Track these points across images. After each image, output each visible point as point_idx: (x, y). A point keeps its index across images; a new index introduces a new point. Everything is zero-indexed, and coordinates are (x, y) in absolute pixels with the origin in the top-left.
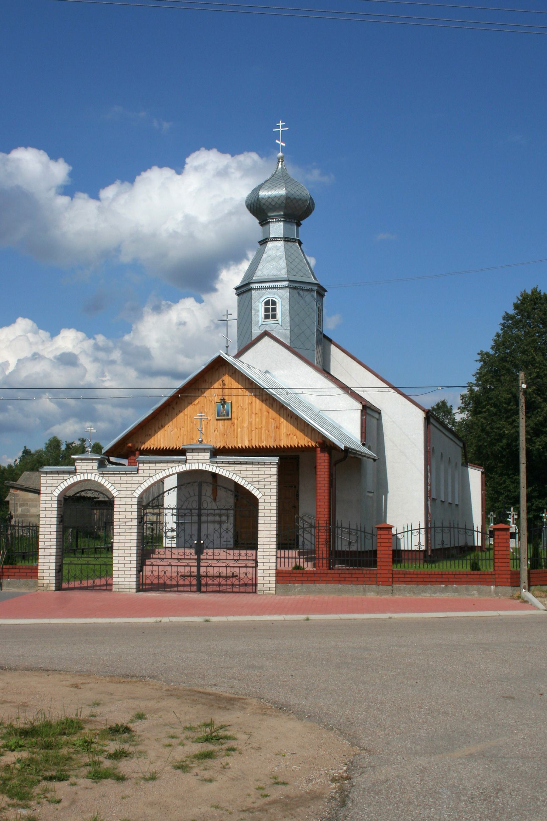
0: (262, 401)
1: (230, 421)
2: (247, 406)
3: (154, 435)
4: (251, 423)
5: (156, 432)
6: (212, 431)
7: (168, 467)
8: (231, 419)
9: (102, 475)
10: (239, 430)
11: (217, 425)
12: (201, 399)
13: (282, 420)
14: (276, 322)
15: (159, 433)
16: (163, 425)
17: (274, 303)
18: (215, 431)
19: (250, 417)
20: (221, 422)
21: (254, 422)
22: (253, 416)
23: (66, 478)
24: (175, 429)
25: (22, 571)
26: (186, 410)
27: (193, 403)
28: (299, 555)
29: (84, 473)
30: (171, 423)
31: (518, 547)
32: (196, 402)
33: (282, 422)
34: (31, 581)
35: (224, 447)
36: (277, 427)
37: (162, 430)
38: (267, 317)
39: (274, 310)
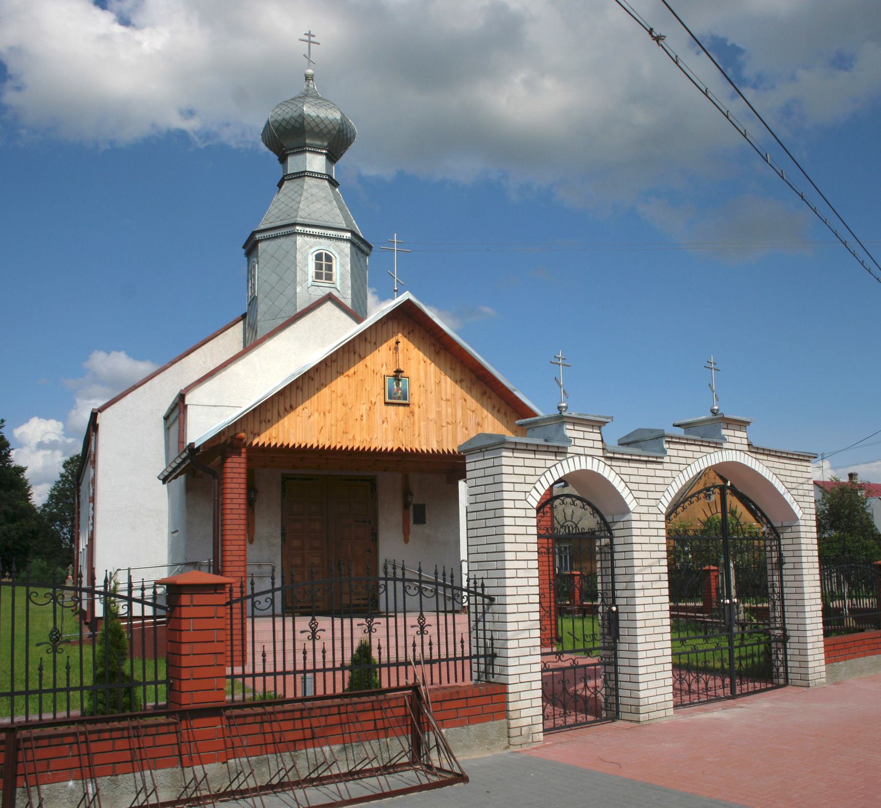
0: (456, 382)
1: (407, 408)
2: (433, 388)
3: (278, 421)
4: (439, 413)
5: (280, 417)
6: (380, 422)
7: (701, 454)
8: (408, 405)
9: (609, 463)
10: (422, 424)
11: (386, 412)
12: (360, 366)
13: (485, 412)
14: (333, 286)
15: (286, 418)
16: (294, 406)
17: (329, 258)
18: (383, 422)
19: (438, 405)
20: (392, 409)
21: (444, 412)
22: (444, 403)
23: (549, 464)
24: (316, 414)
25: (472, 702)
26: (334, 383)
27: (346, 374)
28: (721, 632)
29: (579, 455)
30: (307, 403)
31: (249, 621)
32: (352, 371)
33: (486, 417)
34: (493, 727)
35: (399, 449)
36: (478, 424)
37: (292, 415)
38: (318, 276)
39: (330, 268)
